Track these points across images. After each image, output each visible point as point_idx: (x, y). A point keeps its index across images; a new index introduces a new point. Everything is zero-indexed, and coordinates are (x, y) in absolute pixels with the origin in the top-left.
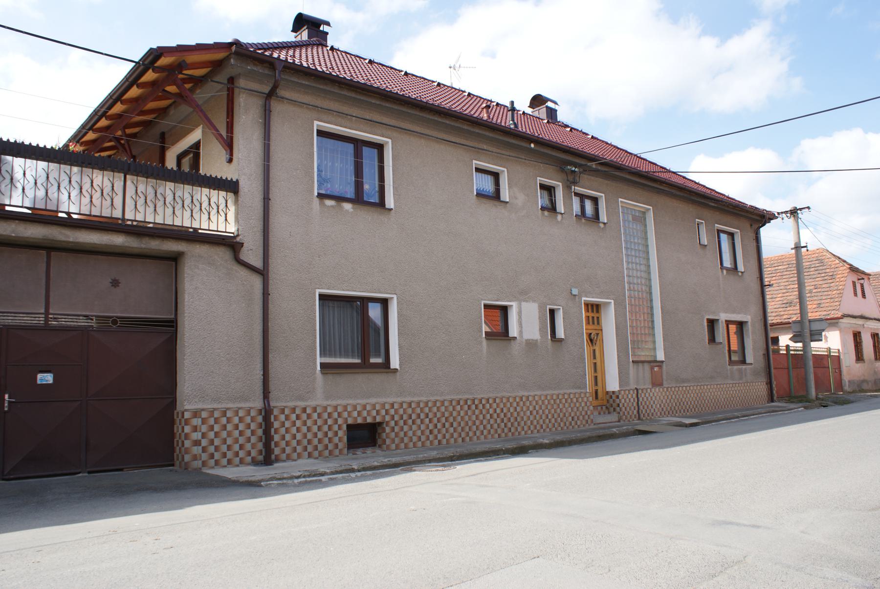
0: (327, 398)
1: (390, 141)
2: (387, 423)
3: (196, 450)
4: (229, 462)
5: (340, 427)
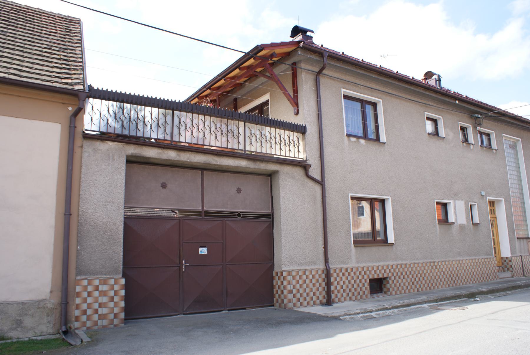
0: (358, 262)
1: (381, 100)
2: (390, 277)
3: (290, 296)
4: (308, 303)
5: (366, 281)
